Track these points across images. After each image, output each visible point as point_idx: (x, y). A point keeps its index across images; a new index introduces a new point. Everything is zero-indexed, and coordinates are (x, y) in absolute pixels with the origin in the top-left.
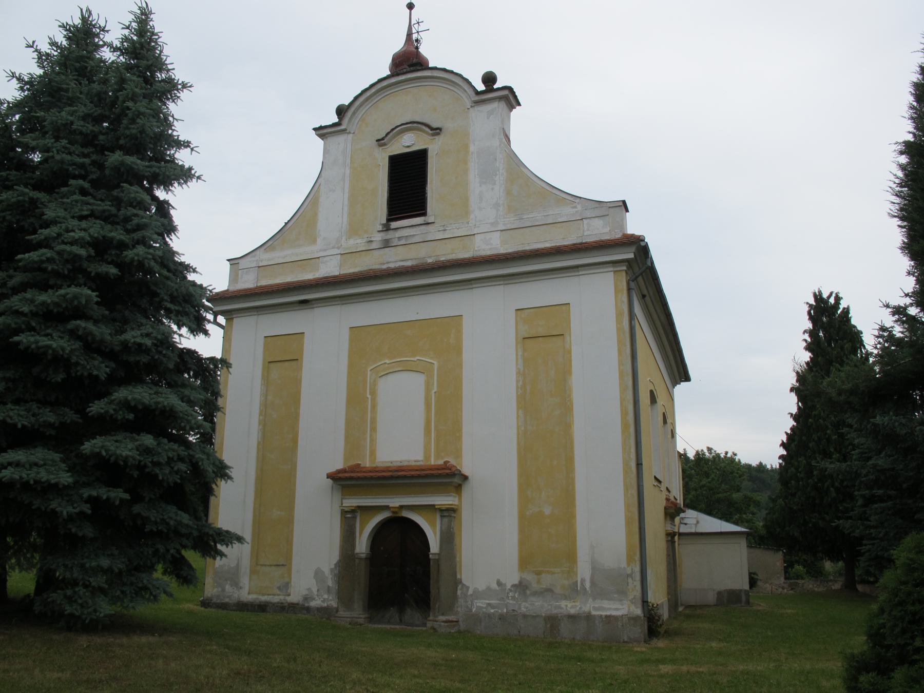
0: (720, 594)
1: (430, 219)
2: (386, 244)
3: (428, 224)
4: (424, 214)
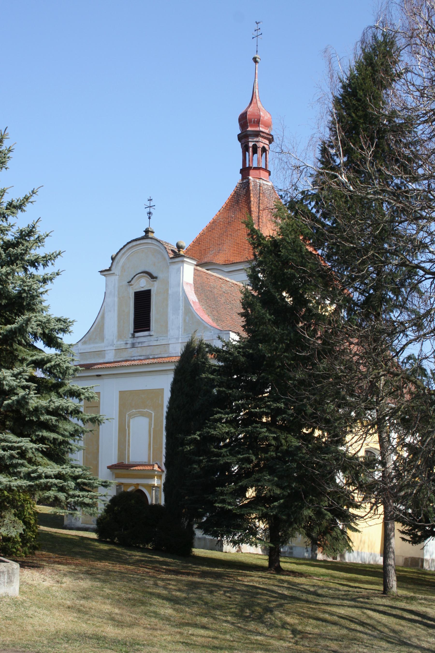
0: (406, 559)
1: (152, 333)
2: (133, 345)
3: (151, 336)
4: (149, 330)
